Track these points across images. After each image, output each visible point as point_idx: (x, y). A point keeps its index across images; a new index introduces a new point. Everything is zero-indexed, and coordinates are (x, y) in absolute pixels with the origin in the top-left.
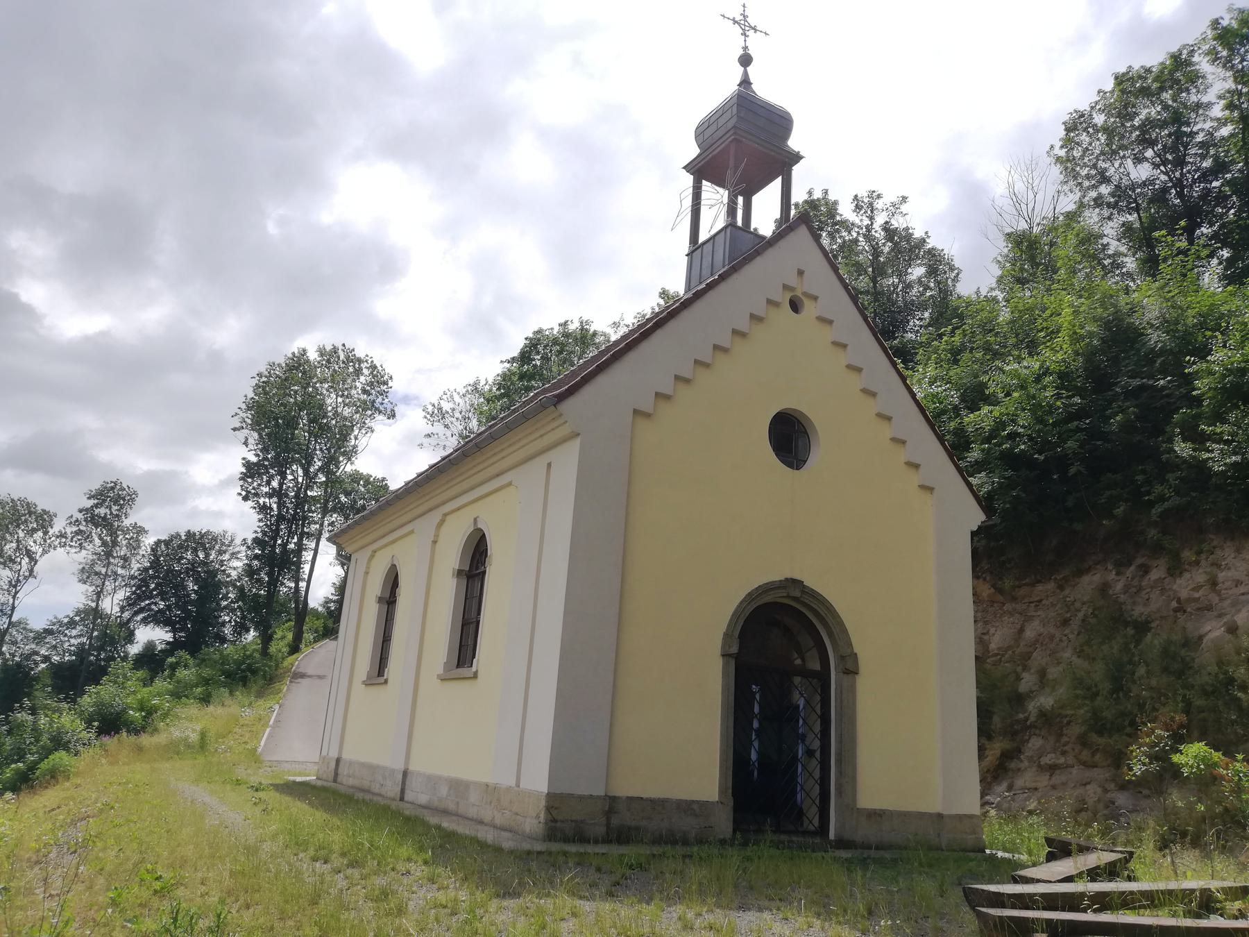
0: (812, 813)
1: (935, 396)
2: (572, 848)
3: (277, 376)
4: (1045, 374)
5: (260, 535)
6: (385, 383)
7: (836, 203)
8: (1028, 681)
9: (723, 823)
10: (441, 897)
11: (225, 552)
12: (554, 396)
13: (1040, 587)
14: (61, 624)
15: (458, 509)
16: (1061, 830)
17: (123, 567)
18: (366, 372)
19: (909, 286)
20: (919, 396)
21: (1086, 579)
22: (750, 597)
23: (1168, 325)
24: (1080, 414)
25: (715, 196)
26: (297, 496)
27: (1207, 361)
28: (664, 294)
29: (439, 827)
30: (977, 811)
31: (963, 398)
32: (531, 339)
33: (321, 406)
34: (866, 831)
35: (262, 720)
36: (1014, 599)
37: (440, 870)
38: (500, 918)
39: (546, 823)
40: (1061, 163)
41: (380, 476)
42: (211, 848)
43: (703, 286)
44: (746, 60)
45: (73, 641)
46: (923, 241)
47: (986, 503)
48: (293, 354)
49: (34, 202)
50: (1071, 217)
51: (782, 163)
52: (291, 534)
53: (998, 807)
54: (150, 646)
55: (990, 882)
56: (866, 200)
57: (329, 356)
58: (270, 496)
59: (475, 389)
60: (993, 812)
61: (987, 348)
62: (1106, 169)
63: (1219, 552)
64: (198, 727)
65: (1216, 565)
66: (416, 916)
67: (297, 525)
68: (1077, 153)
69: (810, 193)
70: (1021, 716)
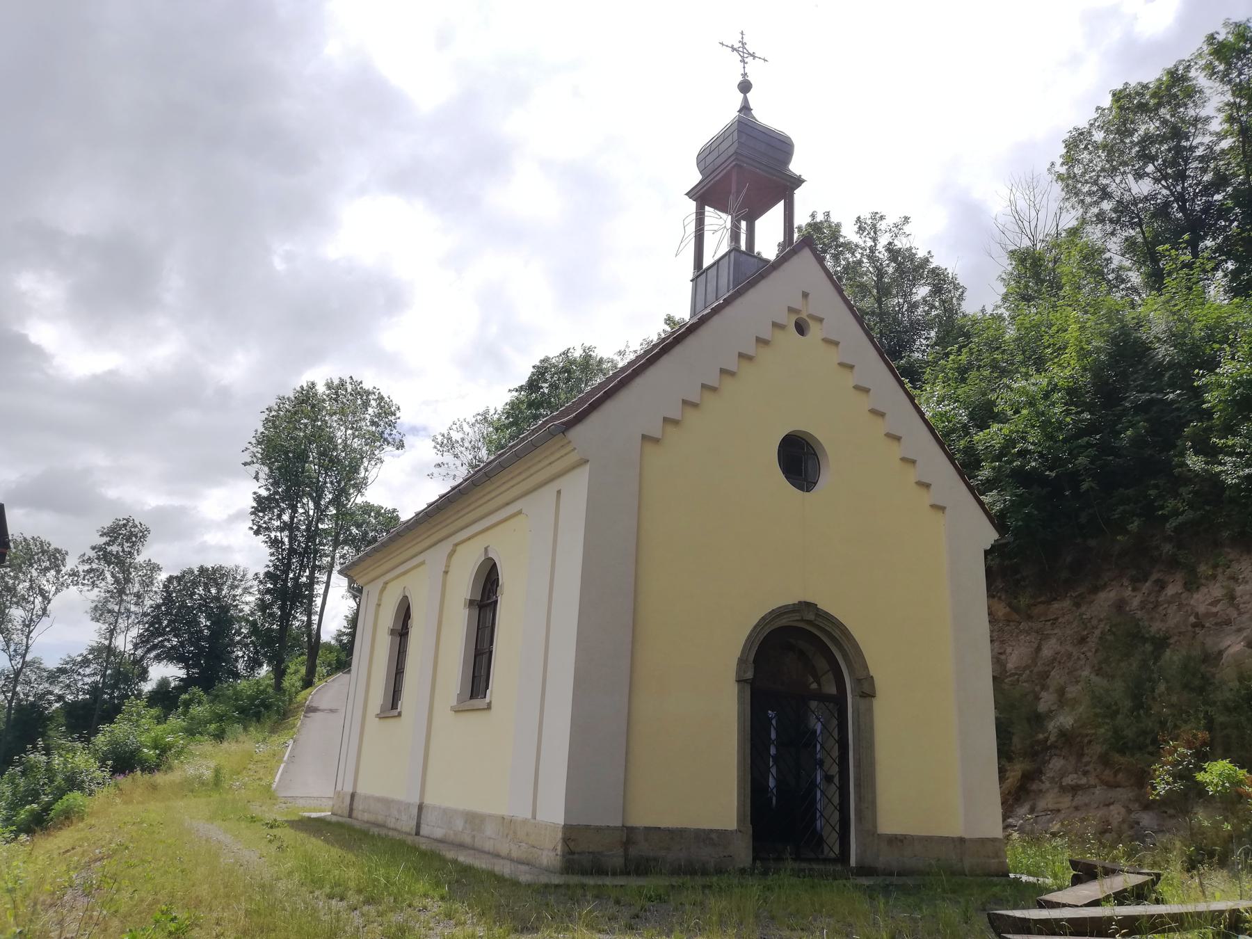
0: (833, 839)
2: (590, 881)
3: (287, 411)
4: (1053, 390)
5: (271, 569)
7: (838, 225)
8: (1047, 701)
9: (742, 851)
11: (237, 587)
13: (1056, 605)
14: (74, 663)
15: (469, 539)
16: (1086, 852)
17: (136, 604)
18: (373, 403)
19: (913, 306)
20: (928, 415)
21: (1102, 595)
23: (1176, 338)
24: (1091, 429)
25: (718, 222)
26: (308, 529)
27: (1216, 374)
28: (669, 320)
29: (455, 862)
30: (998, 832)
31: (972, 417)
33: (331, 439)
34: (886, 858)
35: (276, 756)
36: (1030, 617)
37: (458, 905)
39: (563, 856)
40: (1062, 180)
41: (390, 507)
43: (708, 310)
44: (745, 87)
45: (87, 680)
46: (926, 261)
47: (999, 521)
48: (302, 387)
49: (45, 245)
50: (1074, 232)
52: (303, 567)
53: (1021, 830)
54: (164, 683)
55: (1015, 907)
56: (869, 222)
57: (336, 389)
58: (281, 529)
59: (485, 419)
61: (994, 366)
63: (1235, 567)
64: (212, 764)
65: (1234, 578)
67: (309, 558)
68: (1078, 170)
69: (813, 216)
70: (1041, 736)
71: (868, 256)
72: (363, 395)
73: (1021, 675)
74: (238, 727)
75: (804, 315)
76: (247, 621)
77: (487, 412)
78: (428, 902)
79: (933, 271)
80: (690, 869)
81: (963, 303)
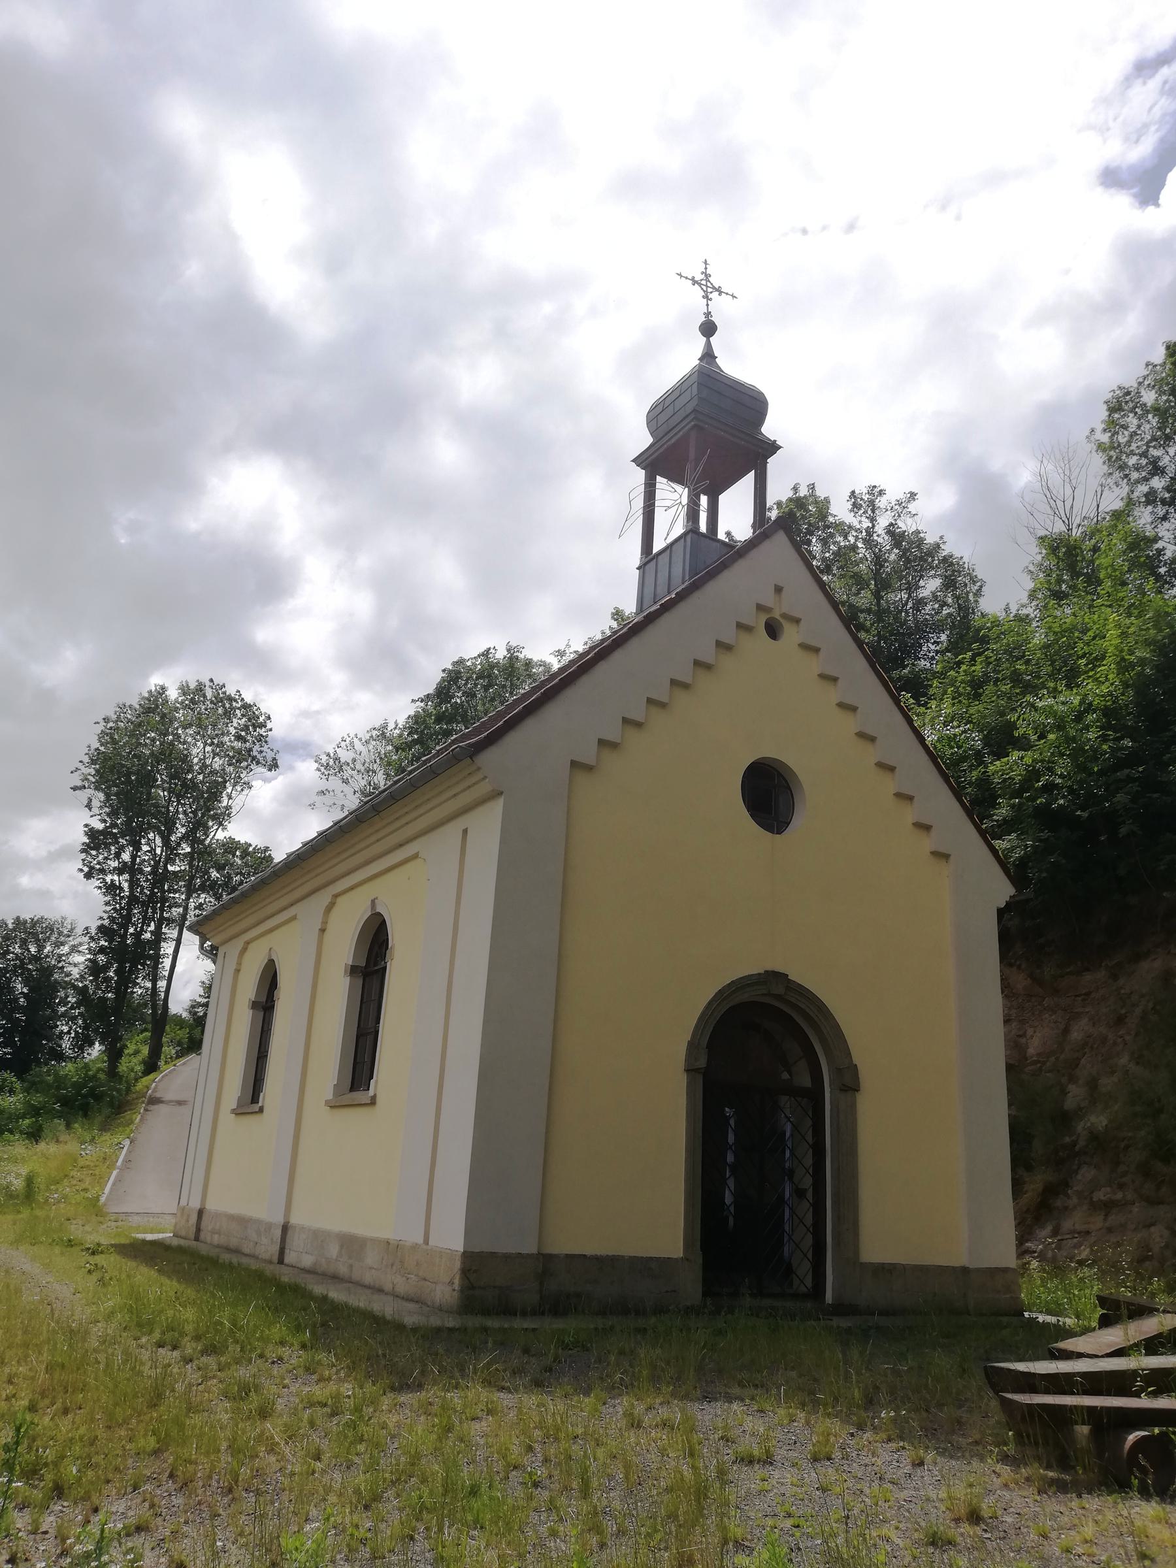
0: (804, 1269)
1: (952, 739)
2: (493, 1323)
3: (129, 721)
5: (106, 922)
6: (263, 725)
7: (827, 501)
8: (1075, 1095)
9: (690, 1286)
10: (319, 1392)
11: (63, 944)
12: (470, 745)
13: (1088, 977)
15: (352, 888)
16: (1118, 1285)
19: (920, 603)
20: (931, 738)
21: (1145, 965)
22: (722, 995)
24: (1132, 760)
25: (672, 497)
26: (154, 872)
28: (617, 615)
29: (325, 1298)
30: (1011, 1262)
31: (986, 741)
32: (450, 671)
33: (185, 758)
35: (107, 1161)
37: (322, 1356)
38: (392, 1420)
39: (462, 1291)
40: (1104, 450)
41: (261, 845)
42: (25, 1332)
43: (656, 607)
44: (708, 329)
46: (937, 546)
47: (1017, 872)
50: (1117, 515)
51: (756, 454)
52: (146, 920)
53: (1042, 1257)
55: (1021, 1360)
56: (866, 497)
57: (194, 694)
58: (119, 871)
59: (382, 734)
60: (1035, 1264)
61: (1016, 678)
62: (1159, 458)
64: (24, 1171)
66: (285, 1418)
68: (1122, 438)
69: (795, 489)
70: (1067, 1139)
71: (865, 541)
72: (226, 704)
73: (1044, 1063)
74: (60, 1123)
75: (776, 615)
76: (75, 987)
77: (385, 726)
78: (285, 1352)
79: (945, 560)
80: (623, 1308)
81: (981, 600)
